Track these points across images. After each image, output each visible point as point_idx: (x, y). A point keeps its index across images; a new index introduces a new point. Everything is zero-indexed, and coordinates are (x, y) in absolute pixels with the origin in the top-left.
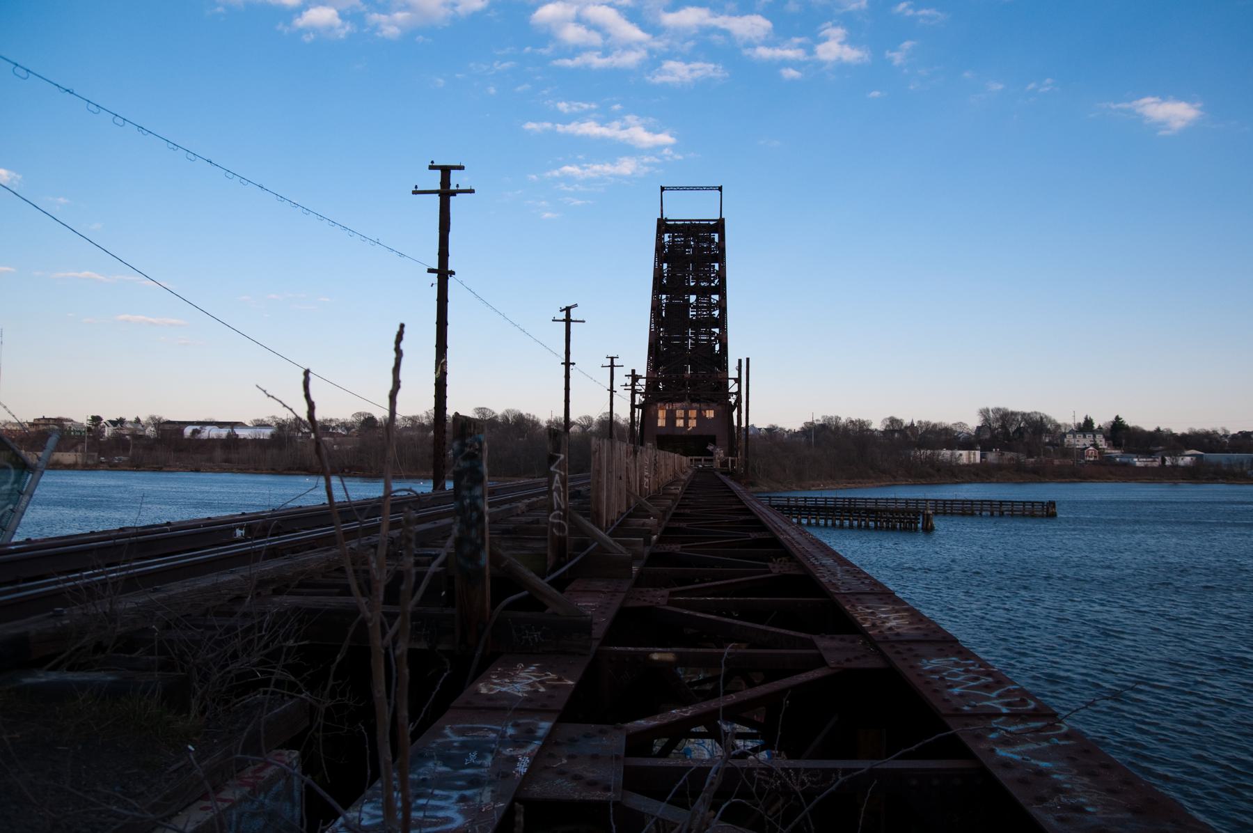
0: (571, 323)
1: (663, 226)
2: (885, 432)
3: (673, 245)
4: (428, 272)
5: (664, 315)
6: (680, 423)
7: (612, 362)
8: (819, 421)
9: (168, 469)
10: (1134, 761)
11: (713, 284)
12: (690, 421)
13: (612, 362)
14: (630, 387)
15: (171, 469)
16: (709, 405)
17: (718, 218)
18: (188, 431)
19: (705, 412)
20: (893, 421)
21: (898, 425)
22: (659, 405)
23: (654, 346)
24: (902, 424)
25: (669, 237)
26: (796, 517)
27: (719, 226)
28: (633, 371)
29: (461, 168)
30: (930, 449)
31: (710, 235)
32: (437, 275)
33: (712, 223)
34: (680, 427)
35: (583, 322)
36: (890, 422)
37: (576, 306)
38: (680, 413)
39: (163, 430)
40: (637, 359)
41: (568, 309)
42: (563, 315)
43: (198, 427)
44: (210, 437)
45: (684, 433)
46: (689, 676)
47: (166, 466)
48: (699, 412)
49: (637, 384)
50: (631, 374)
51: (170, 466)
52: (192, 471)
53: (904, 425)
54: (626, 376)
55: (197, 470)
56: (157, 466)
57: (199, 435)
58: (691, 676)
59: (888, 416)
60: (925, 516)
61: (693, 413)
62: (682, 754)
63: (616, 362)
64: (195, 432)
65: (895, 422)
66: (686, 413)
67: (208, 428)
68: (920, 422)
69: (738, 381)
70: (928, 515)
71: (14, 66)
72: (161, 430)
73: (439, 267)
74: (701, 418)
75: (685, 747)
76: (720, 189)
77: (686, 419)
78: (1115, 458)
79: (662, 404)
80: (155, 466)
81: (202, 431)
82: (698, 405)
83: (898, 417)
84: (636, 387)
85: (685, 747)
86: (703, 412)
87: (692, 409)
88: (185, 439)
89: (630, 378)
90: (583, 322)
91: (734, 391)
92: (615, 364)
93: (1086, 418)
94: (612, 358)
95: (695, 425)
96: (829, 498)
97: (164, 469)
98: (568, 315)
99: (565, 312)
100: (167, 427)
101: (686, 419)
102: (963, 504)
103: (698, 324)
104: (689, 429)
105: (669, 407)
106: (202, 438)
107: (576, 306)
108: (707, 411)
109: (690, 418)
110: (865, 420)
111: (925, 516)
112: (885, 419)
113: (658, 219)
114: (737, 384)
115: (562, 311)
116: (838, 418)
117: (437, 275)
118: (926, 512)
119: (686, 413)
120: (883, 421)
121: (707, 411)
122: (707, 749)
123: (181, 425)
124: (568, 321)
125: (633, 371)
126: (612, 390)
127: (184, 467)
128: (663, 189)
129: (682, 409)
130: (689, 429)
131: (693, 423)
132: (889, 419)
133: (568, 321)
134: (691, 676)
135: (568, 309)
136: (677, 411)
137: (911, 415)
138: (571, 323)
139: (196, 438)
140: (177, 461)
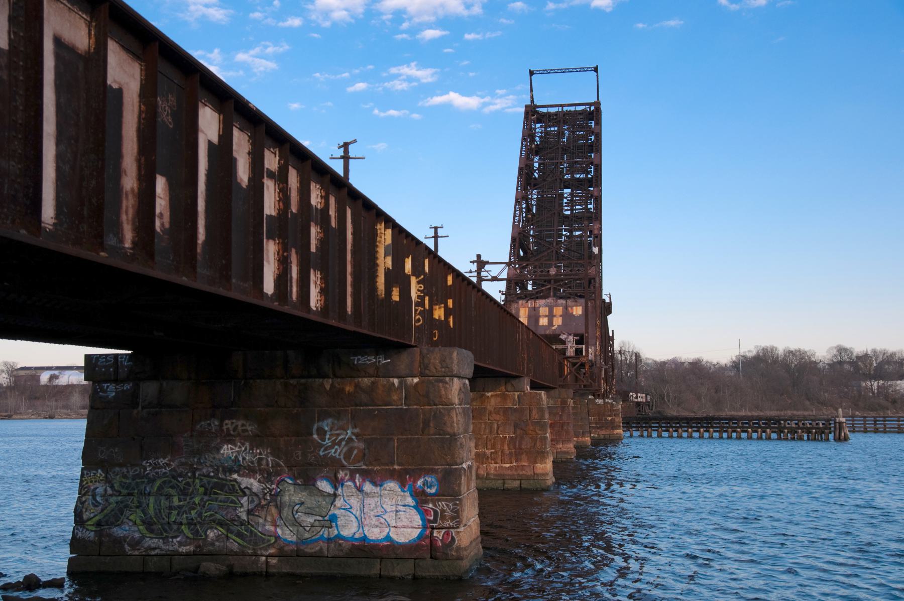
0: (350, 160)
1: (532, 113)
2: (832, 365)
3: (546, 135)
5: (534, 211)
6: (544, 321)
7: (436, 232)
8: (752, 352)
9: (18, 417)
11: (589, 176)
12: (555, 319)
13: (436, 232)
14: (475, 274)
15: (22, 417)
16: (576, 301)
17: (593, 99)
18: (44, 378)
19: (572, 309)
20: (841, 350)
21: (848, 355)
22: (521, 302)
23: (517, 239)
24: (852, 353)
26: (687, 431)
27: (593, 113)
28: (479, 256)
30: (883, 380)
31: (588, 123)
34: (543, 326)
35: (363, 158)
36: (838, 351)
37: (355, 141)
38: (544, 311)
39: (16, 377)
41: (346, 146)
42: (341, 152)
43: (56, 372)
44: (70, 383)
45: (548, 332)
46: (336, 432)
47: (16, 413)
48: (566, 308)
49: (483, 270)
50: (475, 259)
51: (21, 413)
52: (45, 418)
53: (855, 354)
54: (471, 262)
55: (51, 417)
56: (6, 414)
57: (57, 381)
58: (338, 432)
59: (835, 344)
60: (837, 424)
61: (558, 311)
62: (327, 521)
63: (440, 232)
64: (53, 377)
65: (843, 351)
66: (551, 311)
67: (68, 373)
68: (874, 351)
70: (840, 423)
72: (15, 376)
74: (567, 316)
75: (330, 513)
76: (596, 69)
77: (551, 316)
79: (524, 302)
80: (4, 414)
81: (61, 376)
82: (564, 302)
83: (847, 345)
84: (483, 274)
85: (330, 513)
86: (569, 309)
87: (557, 306)
88: (42, 386)
89: (476, 264)
92: (439, 234)
94: (436, 228)
95: (560, 323)
97: (14, 417)
98: (346, 151)
99: (342, 149)
100: (22, 373)
101: (551, 316)
102: (899, 421)
103: (572, 221)
104: (553, 328)
105: (532, 304)
106: (60, 384)
107: (355, 141)
108: (574, 308)
109: (555, 316)
110: (807, 349)
111: (837, 424)
112: (831, 348)
113: (526, 106)
115: (340, 147)
116: (773, 349)
118: (837, 419)
119: (551, 311)
120: (828, 350)
121: (574, 308)
122: (355, 515)
123: (38, 371)
125: (479, 256)
127: (37, 414)
128: (532, 73)
129: (546, 306)
130: (553, 328)
131: (558, 321)
132: (835, 348)
134: (338, 432)
135: (346, 146)
136: (541, 309)
137: (860, 345)
138: (350, 160)
139: (54, 384)
140: (28, 409)
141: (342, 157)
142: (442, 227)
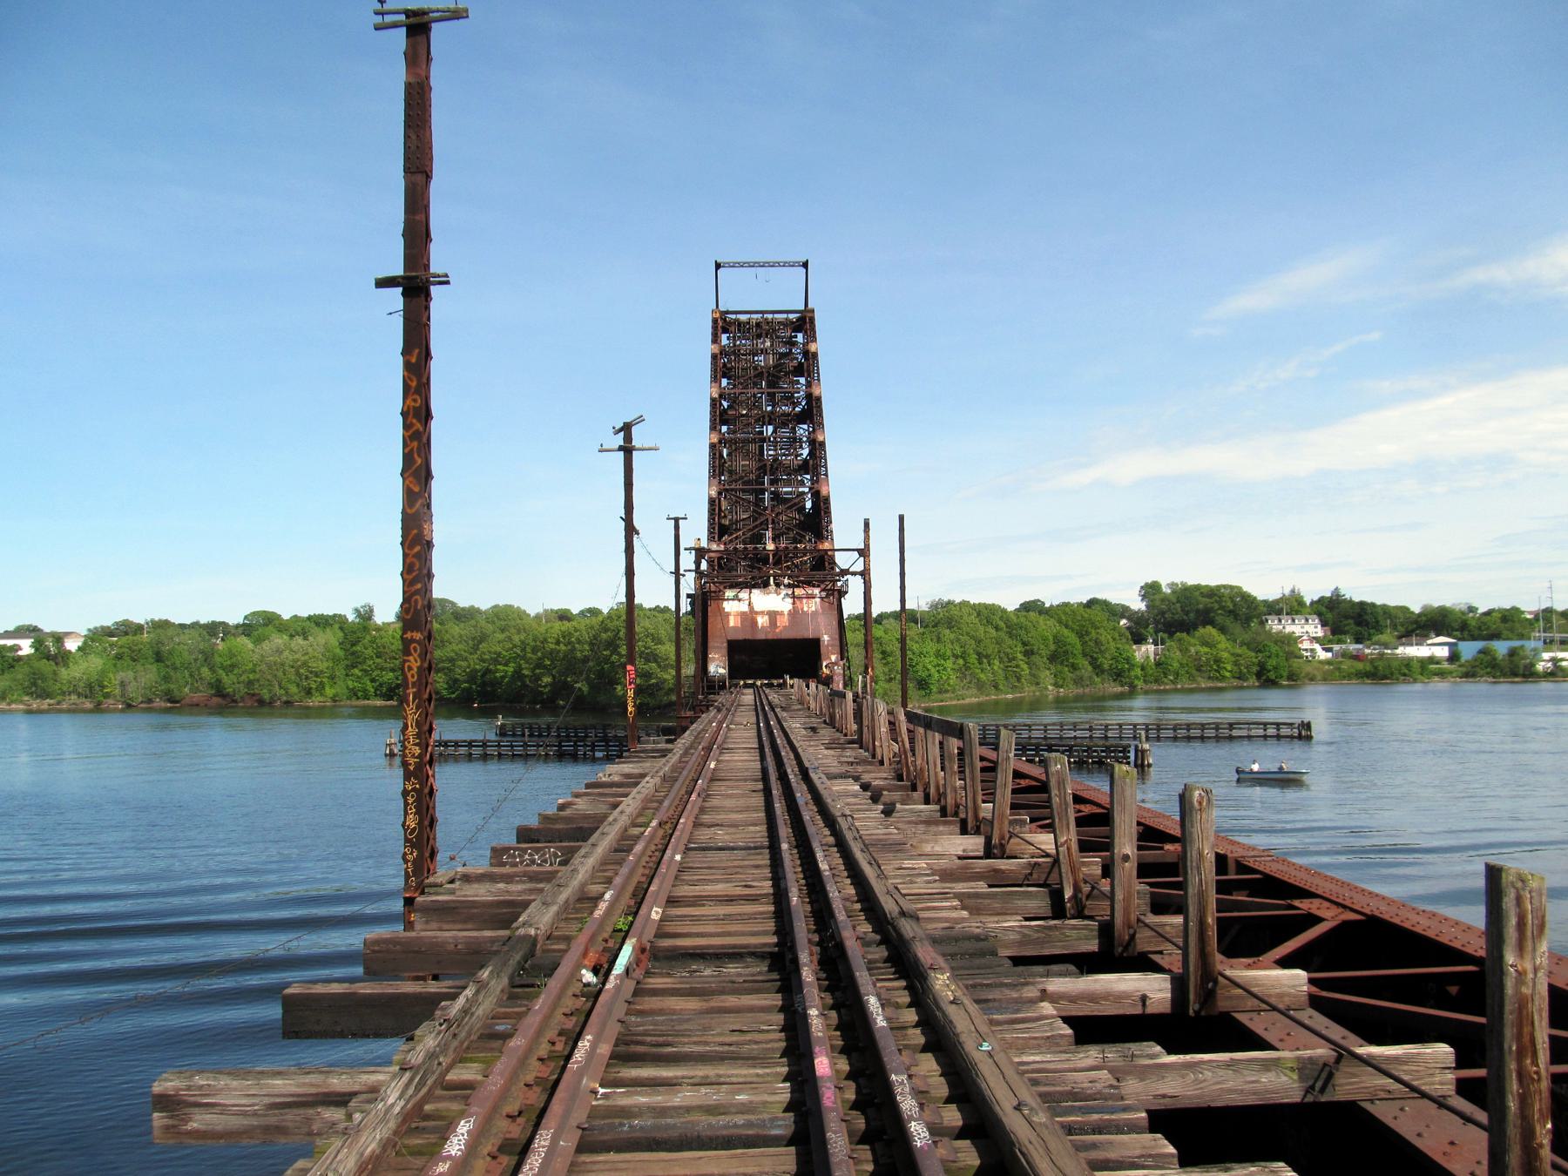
1: (723, 324)
4: (466, 11)
10: (1514, 1075)
25: (728, 338)
27: (805, 322)
29: (457, 15)
32: (400, 289)
33: (792, 316)
35: (901, 518)
37: (640, 419)
40: (697, 530)
41: (627, 429)
42: (619, 440)
69: (864, 553)
71: (784, 1125)
73: (405, 270)
76: (805, 265)
78: (1523, 612)
89: (693, 552)
90: (901, 518)
91: (859, 570)
93: (1293, 591)
96: (1050, 725)
98: (628, 438)
107: (640, 419)
114: (862, 559)
117: (400, 289)
124: (627, 450)
126: (677, 574)
128: (718, 266)
133: (627, 450)
135: (627, 429)
141: (621, 448)
142: (686, 519)
